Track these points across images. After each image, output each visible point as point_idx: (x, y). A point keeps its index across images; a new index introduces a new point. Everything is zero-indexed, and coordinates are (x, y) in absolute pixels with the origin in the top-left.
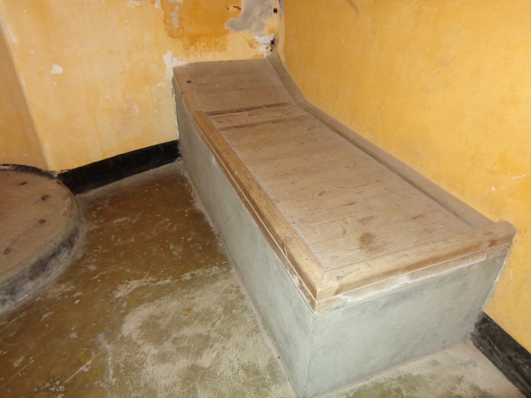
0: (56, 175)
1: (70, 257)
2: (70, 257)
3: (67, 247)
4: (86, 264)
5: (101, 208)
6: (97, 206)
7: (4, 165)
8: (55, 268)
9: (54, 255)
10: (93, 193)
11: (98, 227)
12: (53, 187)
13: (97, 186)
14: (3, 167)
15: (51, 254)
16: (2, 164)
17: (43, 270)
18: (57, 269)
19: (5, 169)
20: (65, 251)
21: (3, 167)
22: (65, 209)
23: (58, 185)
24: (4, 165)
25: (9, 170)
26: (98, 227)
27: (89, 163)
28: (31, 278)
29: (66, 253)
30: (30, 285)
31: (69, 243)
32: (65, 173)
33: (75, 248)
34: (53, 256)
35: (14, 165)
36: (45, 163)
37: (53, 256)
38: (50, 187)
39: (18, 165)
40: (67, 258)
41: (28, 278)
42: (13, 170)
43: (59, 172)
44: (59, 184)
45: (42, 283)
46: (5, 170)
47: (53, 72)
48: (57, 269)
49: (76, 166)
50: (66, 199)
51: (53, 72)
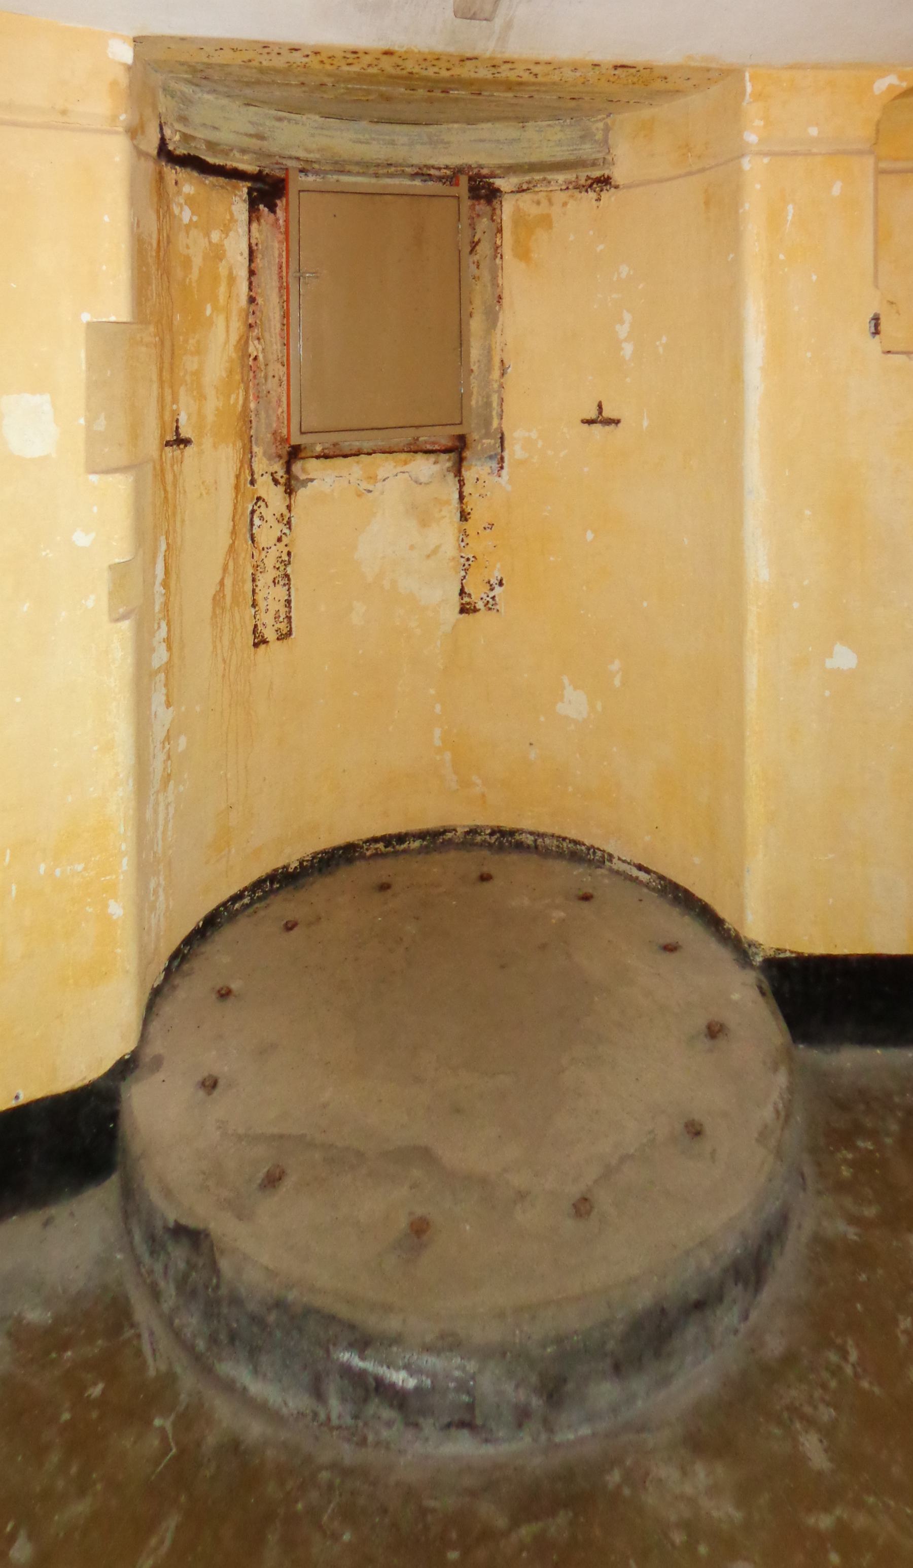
0: (759, 959)
1: (743, 1328)
2: (743, 1328)
3: (746, 1284)
4: (794, 1410)
5: (869, 1146)
6: (858, 1130)
7: (640, 868)
8: (689, 1359)
9: (701, 1305)
10: (853, 1061)
11: (852, 1233)
12: (745, 1000)
13: (865, 1040)
14: (635, 872)
15: (694, 1296)
16: (637, 862)
17: (657, 1354)
18: (696, 1376)
19: (637, 878)
20: (734, 1302)
21: (635, 872)
22: (767, 1113)
23: (760, 999)
24: (640, 868)
25: (647, 885)
26: (852, 1233)
27: (860, 951)
28: (617, 1369)
29: (736, 1310)
30: (604, 1392)
31: (750, 1270)
32: (786, 960)
33: (766, 1296)
34: (699, 1306)
35: (662, 878)
36: (741, 909)
37: (699, 1306)
38: (736, 997)
39: (670, 882)
40: (736, 1332)
41: (609, 1361)
42: (654, 889)
43: (771, 953)
44: (763, 994)
45: (640, 1403)
46: (636, 880)
47: (829, 664)
48: (696, 1376)
49: (819, 949)
50: (775, 1069)
51: (829, 664)
